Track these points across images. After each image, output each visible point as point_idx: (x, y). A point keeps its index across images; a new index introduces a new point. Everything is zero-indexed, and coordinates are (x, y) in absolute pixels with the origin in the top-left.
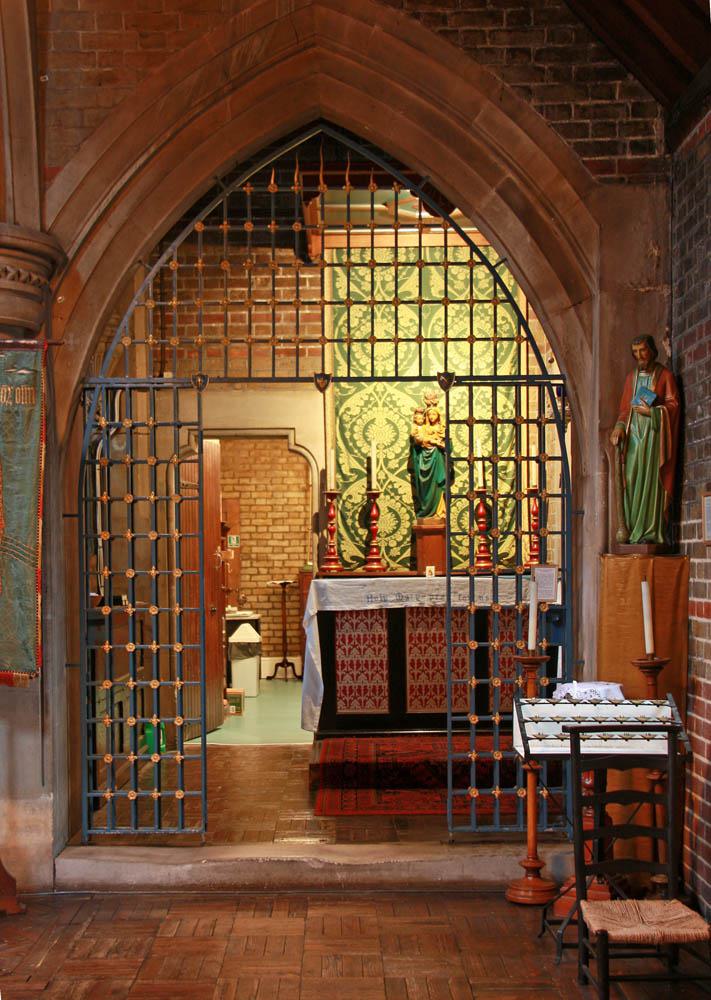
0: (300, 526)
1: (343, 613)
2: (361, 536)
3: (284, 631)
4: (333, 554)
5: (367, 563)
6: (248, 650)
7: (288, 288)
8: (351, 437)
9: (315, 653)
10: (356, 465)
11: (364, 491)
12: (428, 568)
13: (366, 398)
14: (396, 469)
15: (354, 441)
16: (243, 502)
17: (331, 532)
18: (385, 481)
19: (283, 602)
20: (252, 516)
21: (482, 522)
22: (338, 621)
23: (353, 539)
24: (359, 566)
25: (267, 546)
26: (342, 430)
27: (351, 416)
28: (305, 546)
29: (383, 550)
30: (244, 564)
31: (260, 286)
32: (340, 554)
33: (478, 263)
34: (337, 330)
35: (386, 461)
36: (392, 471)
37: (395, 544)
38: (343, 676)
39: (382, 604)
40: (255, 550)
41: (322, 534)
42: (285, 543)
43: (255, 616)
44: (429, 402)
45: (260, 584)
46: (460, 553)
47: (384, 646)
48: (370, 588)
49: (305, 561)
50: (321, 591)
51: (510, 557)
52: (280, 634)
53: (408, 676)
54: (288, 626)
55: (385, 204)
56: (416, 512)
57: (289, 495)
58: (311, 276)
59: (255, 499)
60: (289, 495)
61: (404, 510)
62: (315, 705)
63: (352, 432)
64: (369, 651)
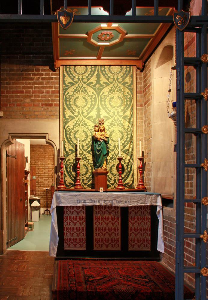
0: (51, 174)
1: (67, 207)
2: (73, 175)
3: (47, 202)
4: (62, 182)
5: (75, 186)
6: (36, 208)
7: (46, 81)
8: (70, 137)
9: (55, 224)
10: (71, 148)
11: (74, 158)
12: (101, 188)
13: (75, 122)
14: (87, 150)
15: (71, 139)
16: (36, 167)
17: (62, 173)
18: (82, 154)
19: (47, 194)
20: (39, 171)
21: (120, 171)
22: (65, 210)
23: (70, 176)
24: (72, 187)
25: (43, 179)
26: (66, 134)
27: (70, 129)
28: (53, 180)
29: (81, 180)
30: (37, 184)
31: (36, 80)
32: (65, 181)
33: (29, 231)
34: (65, 96)
35: (83, 146)
36: (85, 150)
37: (86, 178)
38: (67, 233)
39: (84, 204)
40: (39, 180)
41: (58, 174)
42: (48, 178)
43: (39, 198)
44: (100, 123)
45: (41, 189)
46: (111, 182)
47: (84, 221)
48: (79, 197)
49: (53, 183)
50: (58, 198)
51: (130, 184)
52: (46, 202)
53: (94, 235)
54: (48, 204)
55: (86, 34)
56: (94, 166)
57: (49, 166)
58: (55, 77)
59: (40, 167)
60: (49, 166)
61: (89, 165)
62: (55, 246)
63: (70, 135)
64: (78, 223)
